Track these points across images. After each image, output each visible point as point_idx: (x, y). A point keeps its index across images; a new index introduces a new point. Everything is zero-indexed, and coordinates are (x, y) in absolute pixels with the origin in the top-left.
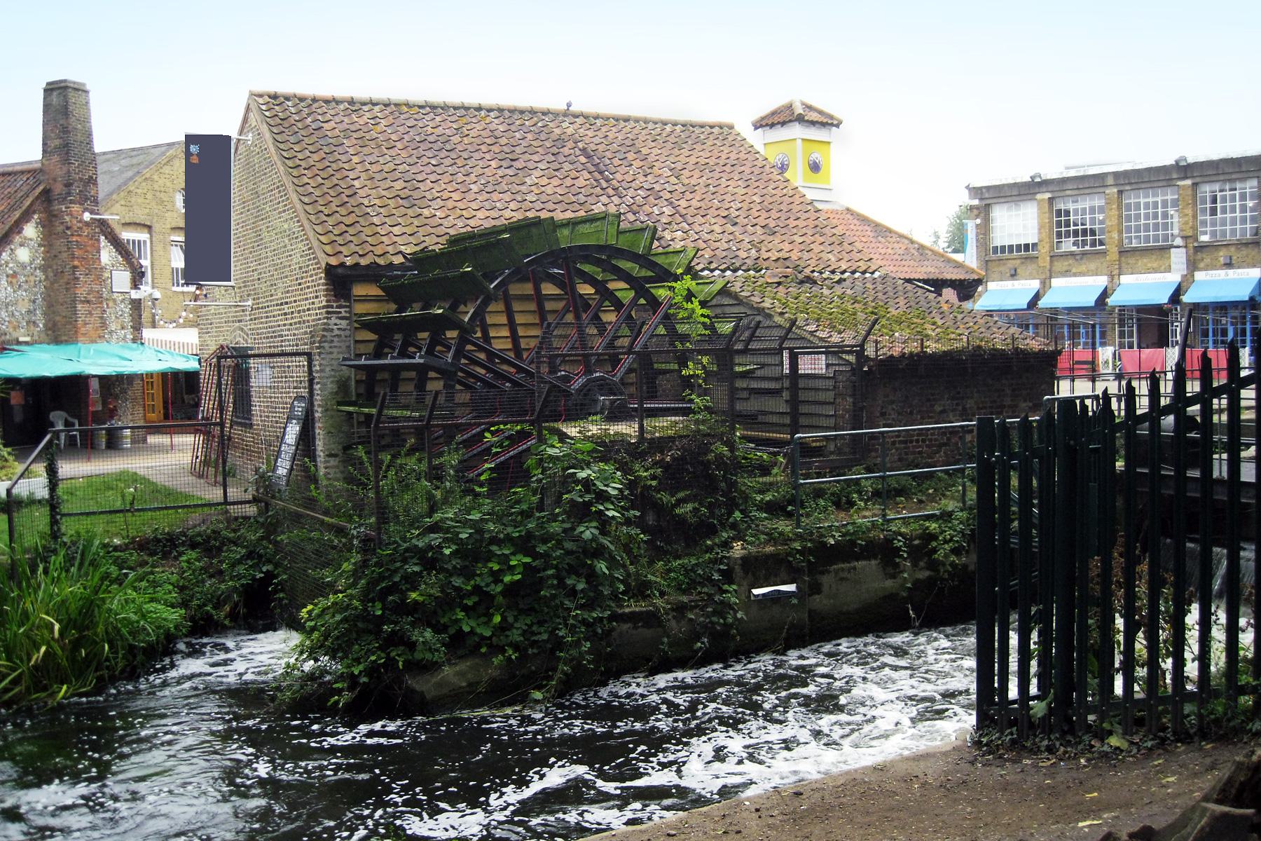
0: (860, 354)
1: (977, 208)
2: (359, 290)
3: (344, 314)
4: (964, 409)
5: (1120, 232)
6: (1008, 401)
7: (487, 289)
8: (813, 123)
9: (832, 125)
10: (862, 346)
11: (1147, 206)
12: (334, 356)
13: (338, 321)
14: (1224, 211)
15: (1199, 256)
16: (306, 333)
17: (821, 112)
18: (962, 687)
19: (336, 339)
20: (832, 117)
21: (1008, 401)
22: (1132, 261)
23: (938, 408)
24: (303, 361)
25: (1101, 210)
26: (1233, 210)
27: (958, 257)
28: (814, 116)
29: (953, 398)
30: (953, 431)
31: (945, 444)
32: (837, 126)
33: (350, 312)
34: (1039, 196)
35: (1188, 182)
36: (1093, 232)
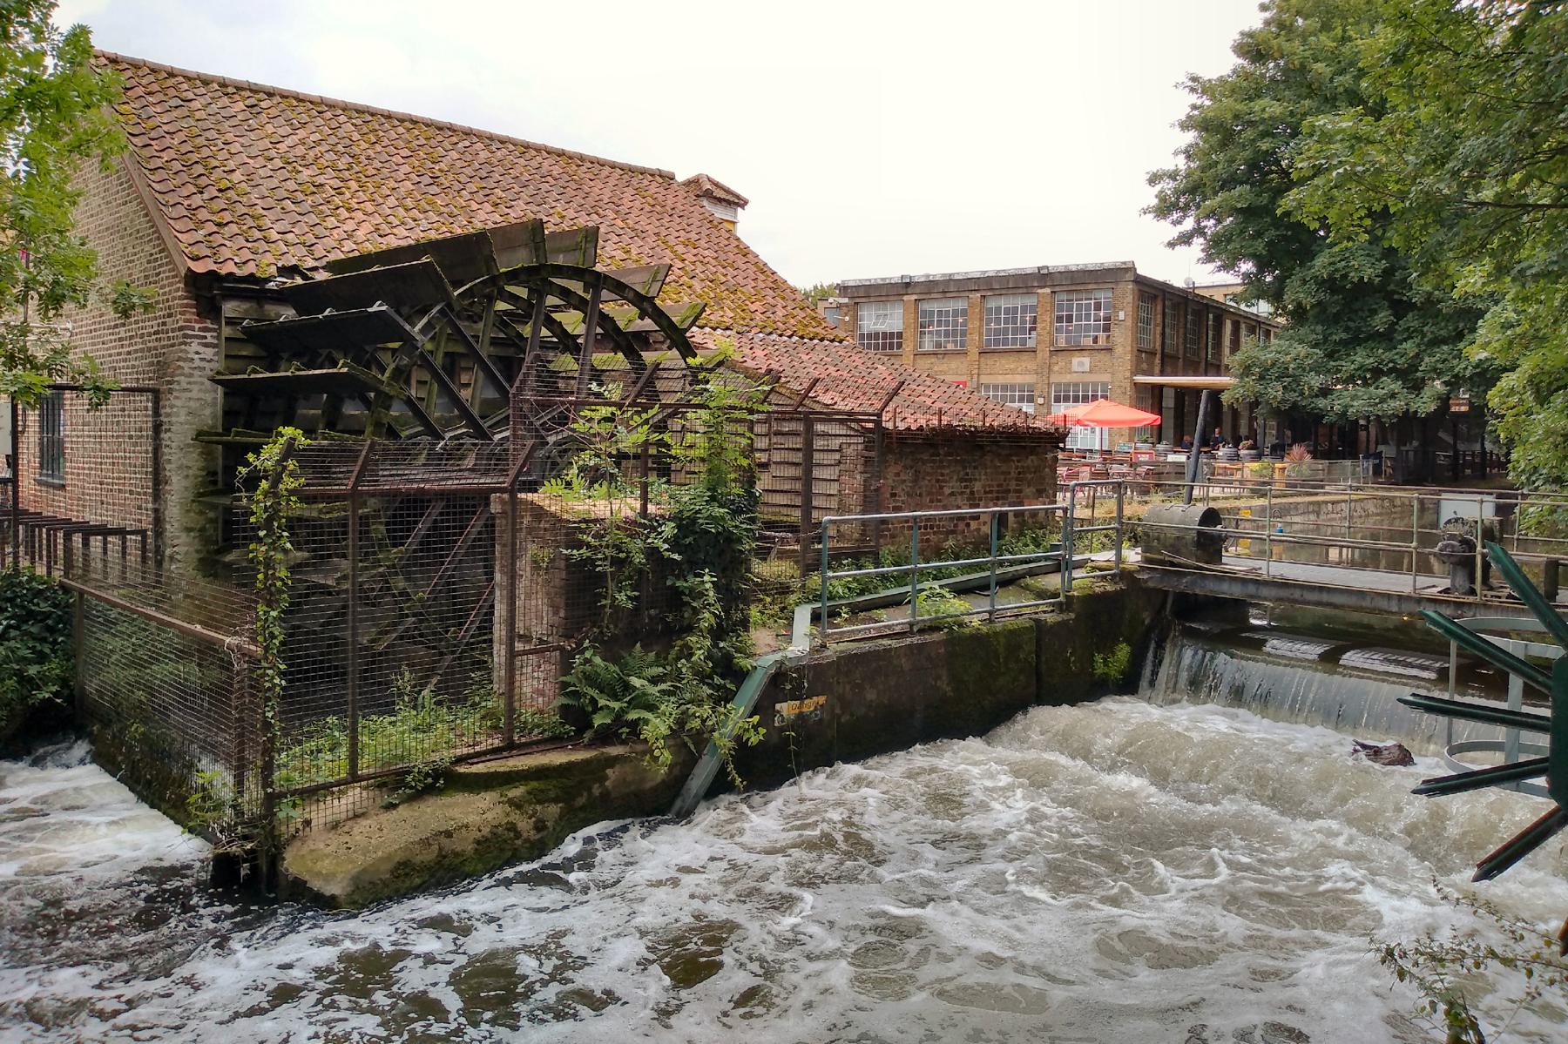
0: (878, 423)
1: (846, 305)
2: (230, 308)
3: (209, 340)
4: (972, 493)
5: (981, 334)
6: (1013, 485)
7: (448, 295)
8: (720, 200)
9: (737, 205)
10: (879, 415)
11: (1007, 311)
12: (194, 394)
13: (201, 349)
14: (1079, 318)
15: (1054, 359)
16: (152, 364)
17: (728, 191)
18: (74, 466)
19: (197, 373)
20: (738, 197)
21: (1013, 485)
22: (990, 362)
23: (947, 491)
24: (145, 401)
25: (964, 313)
26: (1088, 317)
27: (481, 422)
28: (722, 195)
29: (961, 480)
30: (961, 518)
31: (953, 532)
32: (742, 207)
33: (218, 338)
34: (905, 298)
35: (1048, 290)
36: (876, 347)
